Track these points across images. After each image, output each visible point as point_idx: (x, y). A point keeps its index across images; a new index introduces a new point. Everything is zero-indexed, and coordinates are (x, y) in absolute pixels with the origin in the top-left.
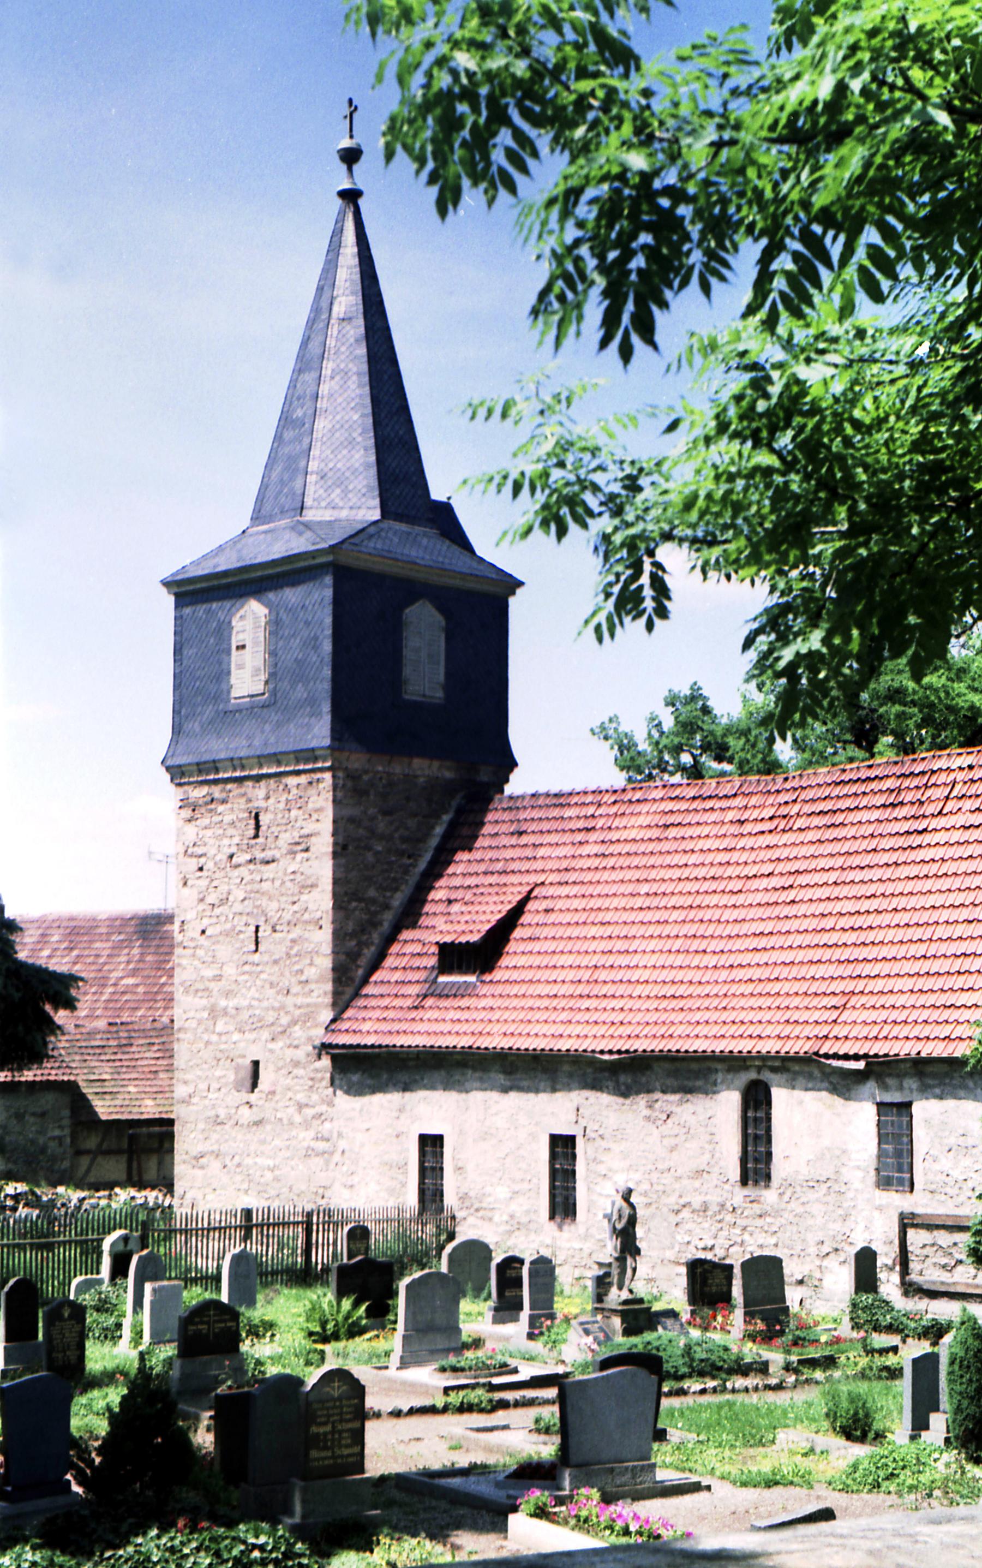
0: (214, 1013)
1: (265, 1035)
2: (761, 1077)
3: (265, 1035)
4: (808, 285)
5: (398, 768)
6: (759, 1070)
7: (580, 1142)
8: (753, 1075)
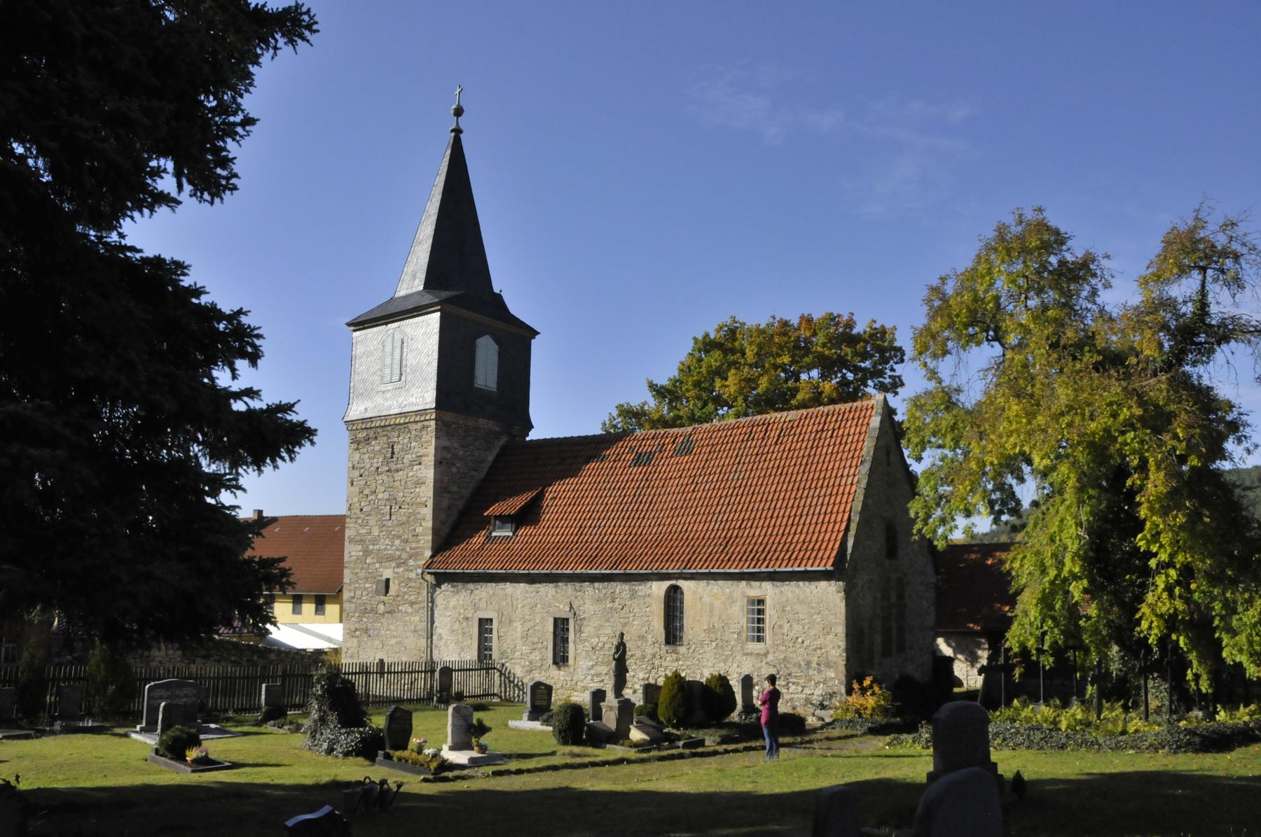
0: (367, 553)
1: (393, 564)
3: (393, 564)
4: (849, 550)
5: (471, 423)
6: (679, 417)
7: (571, 622)
8: (673, 582)
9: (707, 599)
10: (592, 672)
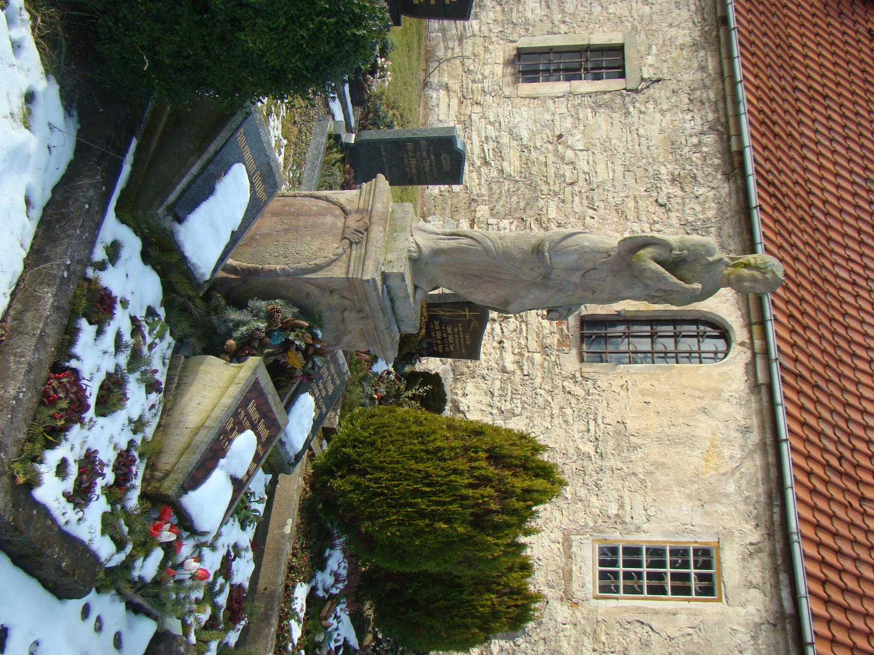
2: (735, 349)
7: (616, 84)
8: (739, 334)
9: (704, 427)
10: (505, 139)
